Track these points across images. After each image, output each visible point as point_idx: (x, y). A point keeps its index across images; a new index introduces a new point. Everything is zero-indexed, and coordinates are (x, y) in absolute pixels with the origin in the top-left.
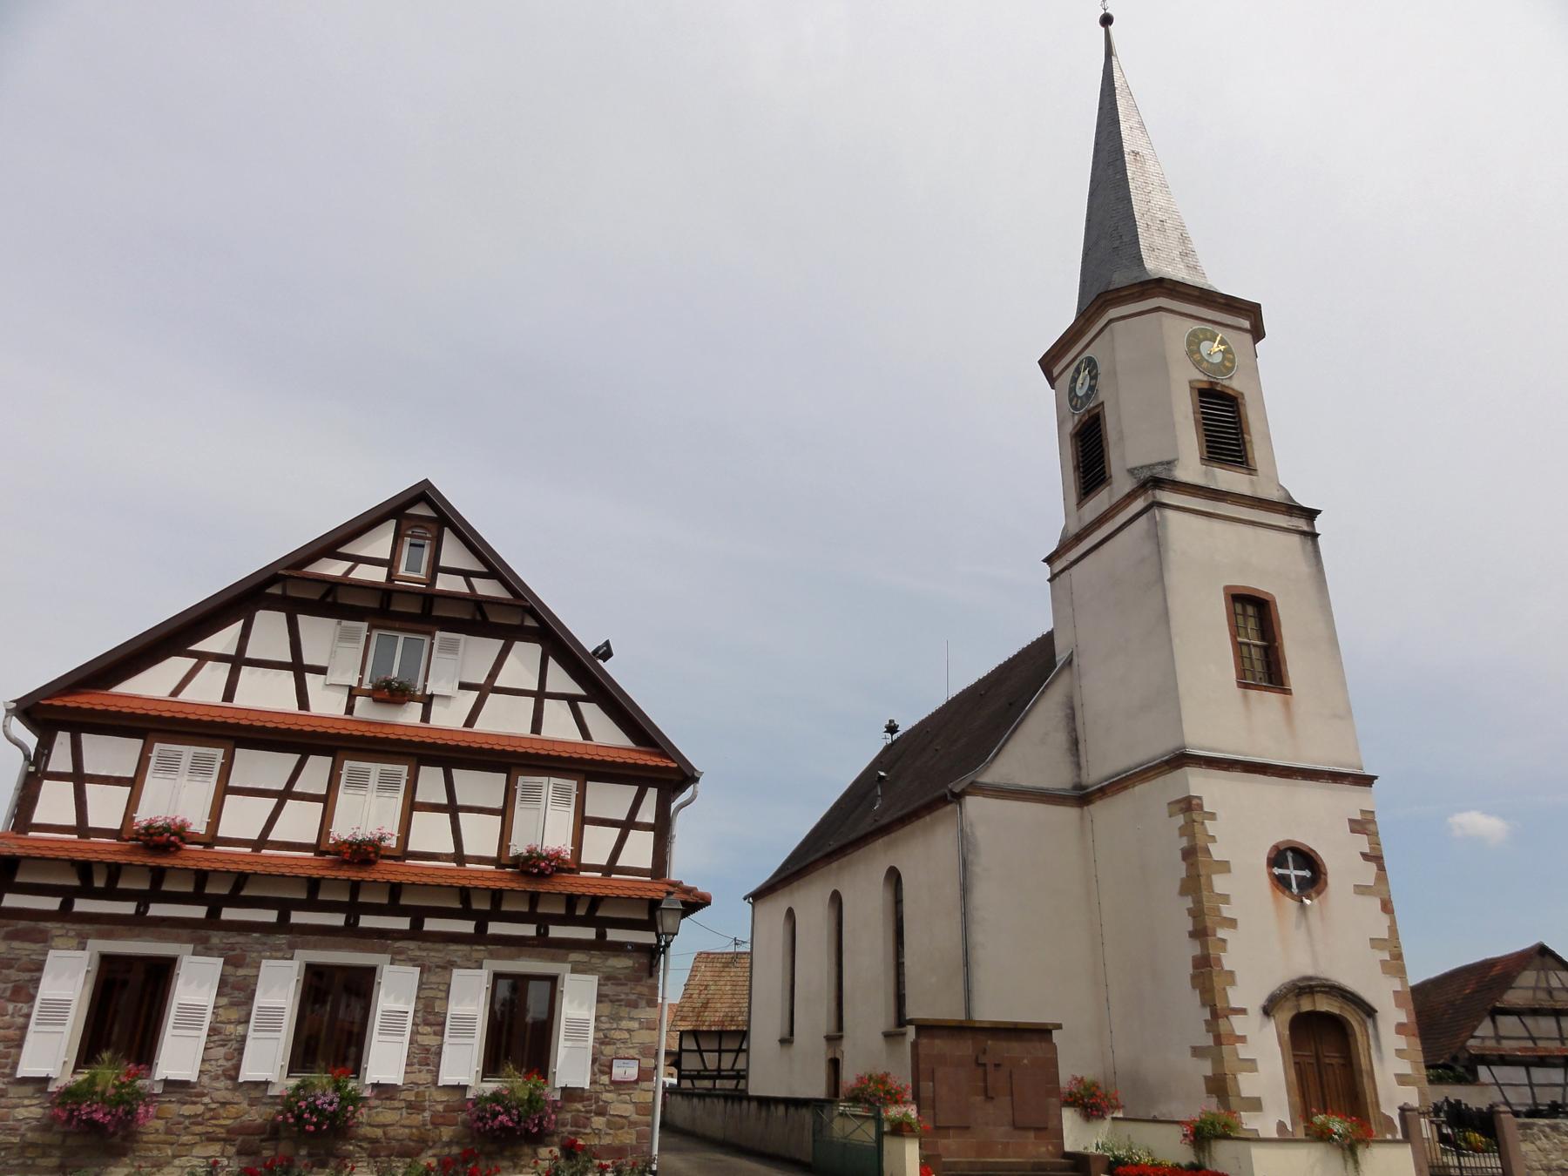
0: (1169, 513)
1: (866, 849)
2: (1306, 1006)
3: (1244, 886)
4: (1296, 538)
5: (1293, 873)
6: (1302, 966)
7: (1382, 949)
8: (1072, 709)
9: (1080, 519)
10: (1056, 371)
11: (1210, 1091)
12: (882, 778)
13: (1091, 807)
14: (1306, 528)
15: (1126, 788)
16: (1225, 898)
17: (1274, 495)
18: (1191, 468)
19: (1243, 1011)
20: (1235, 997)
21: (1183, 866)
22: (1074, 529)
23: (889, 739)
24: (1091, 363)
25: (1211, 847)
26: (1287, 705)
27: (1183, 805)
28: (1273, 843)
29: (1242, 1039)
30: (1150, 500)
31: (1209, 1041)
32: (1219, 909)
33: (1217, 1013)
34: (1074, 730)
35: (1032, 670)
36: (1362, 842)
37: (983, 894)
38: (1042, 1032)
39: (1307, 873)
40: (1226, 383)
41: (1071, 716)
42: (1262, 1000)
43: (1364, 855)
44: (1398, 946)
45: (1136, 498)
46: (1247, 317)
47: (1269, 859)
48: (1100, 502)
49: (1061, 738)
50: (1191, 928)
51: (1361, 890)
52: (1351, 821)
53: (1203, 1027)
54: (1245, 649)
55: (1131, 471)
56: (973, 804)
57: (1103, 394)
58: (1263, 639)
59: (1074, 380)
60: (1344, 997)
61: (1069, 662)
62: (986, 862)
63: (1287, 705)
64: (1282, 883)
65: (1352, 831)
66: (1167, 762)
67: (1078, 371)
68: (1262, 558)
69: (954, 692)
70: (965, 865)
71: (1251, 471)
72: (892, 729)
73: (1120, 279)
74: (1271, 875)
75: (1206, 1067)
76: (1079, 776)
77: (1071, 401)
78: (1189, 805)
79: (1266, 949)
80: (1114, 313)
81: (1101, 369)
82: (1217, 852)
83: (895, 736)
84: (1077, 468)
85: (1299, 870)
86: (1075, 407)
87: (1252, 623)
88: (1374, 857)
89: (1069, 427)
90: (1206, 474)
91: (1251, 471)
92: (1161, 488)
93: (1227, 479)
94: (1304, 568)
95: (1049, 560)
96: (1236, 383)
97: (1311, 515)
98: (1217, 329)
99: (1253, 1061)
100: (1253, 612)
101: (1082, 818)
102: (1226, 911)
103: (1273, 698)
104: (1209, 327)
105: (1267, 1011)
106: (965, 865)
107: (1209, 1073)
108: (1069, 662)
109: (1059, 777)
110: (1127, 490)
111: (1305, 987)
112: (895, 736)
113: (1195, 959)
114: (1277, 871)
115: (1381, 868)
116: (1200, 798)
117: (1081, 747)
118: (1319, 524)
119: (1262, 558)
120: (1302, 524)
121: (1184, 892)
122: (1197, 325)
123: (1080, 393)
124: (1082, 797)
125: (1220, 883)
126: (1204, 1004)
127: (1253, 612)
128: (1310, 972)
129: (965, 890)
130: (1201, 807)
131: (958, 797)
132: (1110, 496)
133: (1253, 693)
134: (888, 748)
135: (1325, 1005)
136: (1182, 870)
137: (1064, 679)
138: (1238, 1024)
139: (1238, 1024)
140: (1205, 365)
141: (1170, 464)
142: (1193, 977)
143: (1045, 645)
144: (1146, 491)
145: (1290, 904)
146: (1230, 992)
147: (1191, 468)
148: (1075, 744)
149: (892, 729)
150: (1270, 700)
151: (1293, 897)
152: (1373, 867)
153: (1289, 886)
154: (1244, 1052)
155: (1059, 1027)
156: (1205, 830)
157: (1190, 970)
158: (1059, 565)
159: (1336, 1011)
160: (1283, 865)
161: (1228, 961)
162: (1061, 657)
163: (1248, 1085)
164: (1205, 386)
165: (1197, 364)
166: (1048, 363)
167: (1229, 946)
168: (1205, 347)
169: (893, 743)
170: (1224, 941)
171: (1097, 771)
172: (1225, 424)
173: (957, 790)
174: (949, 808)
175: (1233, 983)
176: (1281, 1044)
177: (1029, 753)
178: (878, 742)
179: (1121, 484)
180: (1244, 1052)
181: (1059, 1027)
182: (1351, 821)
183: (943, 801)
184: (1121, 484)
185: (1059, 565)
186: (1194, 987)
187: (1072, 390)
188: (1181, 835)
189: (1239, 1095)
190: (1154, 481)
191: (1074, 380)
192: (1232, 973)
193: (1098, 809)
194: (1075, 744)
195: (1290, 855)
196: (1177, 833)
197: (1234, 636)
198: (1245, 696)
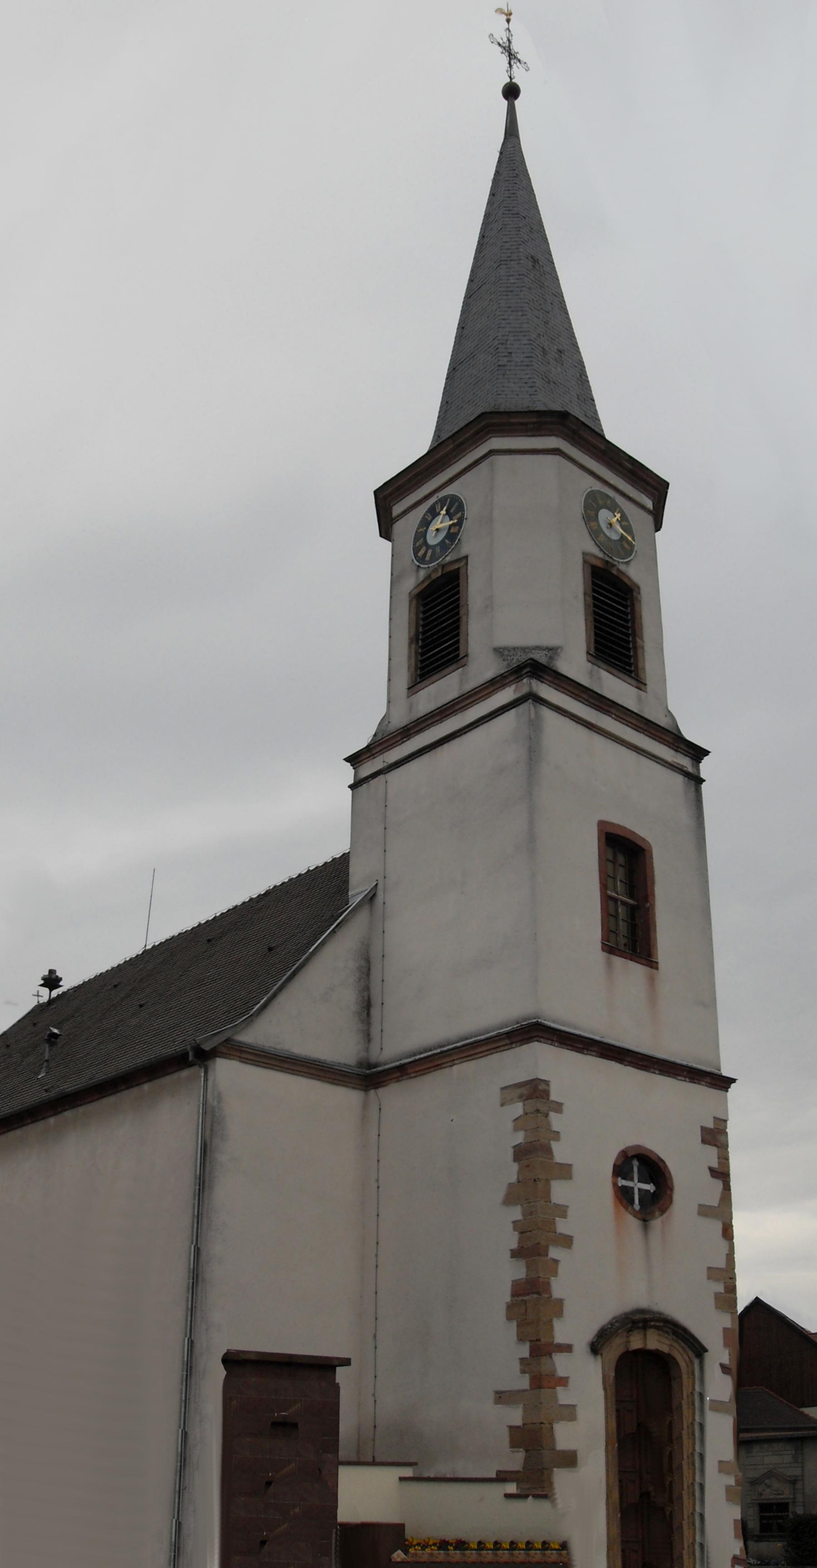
0: (546, 712)
1: (18, 1132)
2: (636, 1343)
3: (586, 1197)
4: (679, 779)
5: (638, 1186)
6: (638, 1296)
7: (717, 1280)
8: (368, 961)
9: (411, 708)
10: (397, 510)
11: (514, 1444)
12: (56, 1036)
13: (381, 1091)
14: (690, 769)
15: (439, 1067)
16: (562, 1211)
17: (663, 722)
18: (575, 663)
19: (567, 1348)
20: (562, 1332)
21: (515, 1167)
22: (400, 720)
23: (45, 994)
24: (455, 507)
25: (554, 1145)
26: (652, 981)
27: (524, 1091)
28: (622, 1147)
29: (563, 1382)
30: (525, 690)
31: (524, 1383)
32: (553, 1223)
33: (540, 1349)
34: (367, 988)
35: (307, 910)
36: (710, 1156)
37: (227, 1191)
38: (324, 1368)
39: (650, 1187)
40: (622, 567)
41: (366, 968)
42: (589, 1333)
43: (711, 1170)
44: (733, 1278)
45: (503, 686)
46: (650, 495)
47: (615, 1166)
48: (446, 687)
49: (349, 997)
50: (514, 1245)
51: (705, 1211)
52: (704, 1130)
53: (517, 1366)
54: (611, 904)
55: (499, 651)
56: (225, 1071)
57: (470, 545)
58: (631, 896)
59: (425, 523)
60: (675, 1333)
61: (371, 898)
62: (233, 1148)
63: (652, 981)
64: (624, 1196)
65: (704, 1141)
66: (509, 1035)
67: (433, 513)
68: (639, 794)
69: (160, 934)
70: (205, 1151)
71: (640, 683)
72: (51, 981)
73: (515, 397)
74: (615, 1184)
75: (515, 1416)
76: (367, 1050)
77: (416, 551)
78: (535, 1091)
79: (603, 1274)
80: (496, 443)
81: (471, 511)
82: (561, 1152)
83: (55, 993)
84: (414, 640)
85: (644, 1183)
86: (422, 560)
87: (621, 874)
88: (721, 1174)
89: (410, 584)
90: (591, 673)
91: (640, 683)
92: (540, 678)
93: (613, 686)
94: (685, 817)
95: (354, 760)
96: (634, 572)
97: (698, 753)
98: (620, 500)
99: (573, 1407)
100: (625, 857)
101: (365, 1106)
102: (562, 1227)
103: (637, 970)
104: (611, 493)
105: (595, 1348)
106: (205, 1151)
107: (518, 1422)
108: (371, 898)
109: (342, 1049)
110: (489, 674)
111: (639, 1320)
112: (55, 993)
113: (515, 1284)
114: (622, 1182)
115: (727, 1188)
116: (547, 1083)
117: (375, 1012)
118: (706, 768)
119: (639, 794)
120: (685, 762)
121: (510, 1199)
122: (598, 486)
123: (433, 539)
124: (369, 1077)
125: (560, 1191)
126: (521, 1339)
127: (625, 857)
128: (643, 1303)
129: (203, 1184)
130: (546, 1093)
131: (203, 1057)
132: (461, 682)
133: (618, 961)
134: (39, 1010)
135: (654, 1342)
136: (512, 1172)
137: (363, 917)
138: (561, 1364)
139: (561, 1364)
140: (602, 538)
141: (553, 651)
142: (510, 1307)
143: (336, 871)
144: (519, 678)
145: (633, 1223)
146: (557, 1325)
147: (575, 663)
148: (366, 1006)
149: (51, 981)
150: (632, 972)
151: (635, 1214)
152: (719, 1184)
153: (632, 1202)
154: (564, 1396)
155: (346, 1362)
156: (549, 1124)
157: (508, 1299)
158: (368, 769)
159: (665, 1349)
160: (627, 1176)
161: (559, 1288)
162: (357, 890)
163: (565, 1437)
164: (599, 564)
165: (595, 533)
166: (388, 498)
167: (561, 1269)
168: (604, 515)
169: (51, 1002)
170: (556, 1262)
171: (396, 1043)
172: (617, 616)
173: (207, 1047)
174: (185, 1073)
175: (559, 1313)
176: (605, 1389)
177: (309, 1013)
178: (28, 996)
179: (481, 666)
180: (564, 1396)
181: (346, 1362)
182: (704, 1130)
183: (178, 1062)
184: (481, 666)
185: (368, 769)
186: (509, 1318)
187: (420, 536)
188: (516, 1129)
189: (553, 1449)
190: (533, 667)
191: (425, 523)
192: (560, 1302)
193: (393, 1096)
194: (366, 1006)
195: (636, 1163)
196: (510, 1125)
197: (604, 887)
198: (609, 965)
